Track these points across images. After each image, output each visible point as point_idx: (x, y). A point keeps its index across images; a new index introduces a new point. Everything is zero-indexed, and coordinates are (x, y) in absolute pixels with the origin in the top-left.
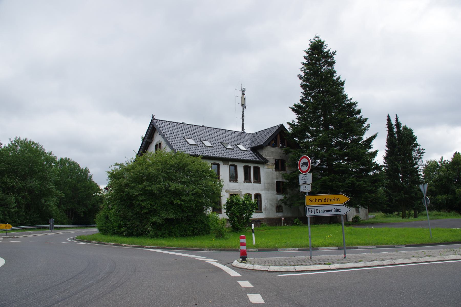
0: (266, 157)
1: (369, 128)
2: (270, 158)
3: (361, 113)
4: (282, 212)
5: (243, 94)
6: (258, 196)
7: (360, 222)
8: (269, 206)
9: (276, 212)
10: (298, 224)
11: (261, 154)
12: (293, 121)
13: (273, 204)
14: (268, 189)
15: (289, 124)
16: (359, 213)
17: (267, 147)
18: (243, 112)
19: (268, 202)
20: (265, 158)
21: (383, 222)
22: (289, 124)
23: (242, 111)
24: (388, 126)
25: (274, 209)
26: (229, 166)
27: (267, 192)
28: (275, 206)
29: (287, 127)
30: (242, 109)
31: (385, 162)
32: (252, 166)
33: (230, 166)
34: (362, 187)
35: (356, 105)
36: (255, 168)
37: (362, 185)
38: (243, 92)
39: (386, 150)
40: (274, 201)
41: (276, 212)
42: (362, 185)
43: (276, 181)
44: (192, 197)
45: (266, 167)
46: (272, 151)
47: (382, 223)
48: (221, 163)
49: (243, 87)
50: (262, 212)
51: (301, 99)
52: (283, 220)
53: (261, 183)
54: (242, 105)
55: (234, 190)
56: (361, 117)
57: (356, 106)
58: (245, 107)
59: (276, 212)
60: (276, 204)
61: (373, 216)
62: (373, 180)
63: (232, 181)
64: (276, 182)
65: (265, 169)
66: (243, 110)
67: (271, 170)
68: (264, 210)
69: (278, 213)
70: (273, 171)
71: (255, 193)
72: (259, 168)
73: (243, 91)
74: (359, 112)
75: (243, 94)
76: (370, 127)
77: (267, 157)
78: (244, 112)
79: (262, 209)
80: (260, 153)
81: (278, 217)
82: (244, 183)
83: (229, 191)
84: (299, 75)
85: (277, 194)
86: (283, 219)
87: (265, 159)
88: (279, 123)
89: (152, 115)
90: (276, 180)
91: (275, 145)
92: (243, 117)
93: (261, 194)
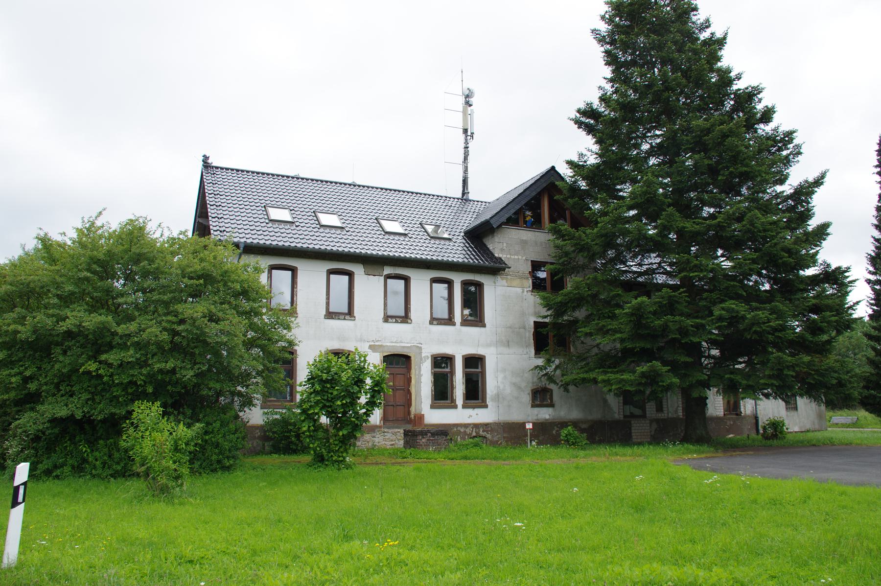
0: (505, 256)
1: (800, 158)
2: (516, 257)
3: (774, 120)
4: (552, 405)
5: (468, 104)
6: (474, 362)
7: (785, 438)
8: (508, 390)
9: (532, 406)
10: (573, 444)
11: (491, 248)
12: (581, 155)
13: (523, 385)
14: (508, 344)
15: (570, 163)
16: (797, 410)
17: (509, 230)
18: (466, 148)
19: (505, 377)
20: (500, 258)
21: (851, 444)
22: (570, 163)
23: (463, 145)
24: (879, 169)
25: (527, 398)
26: (382, 278)
27: (505, 350)
28: (529, 390)
29: (565, 171)
30: (463, 141)
31: (871, 269)
32: (457, 279)
33: (389, 277)
34: (764, 328)
35: (759, 96)
36: (465, 284)
37: (764, 323)
38: (466, 98)
39: (874, 238)
40: (526, 375)
41: (530, 405)
42: (764, 323)
43: (535, 322)
44: (130, 355)
45: (500, 281)
46: (524, 238)
47: (847, 444)
48: (358, 270)
49: (466, 86)
50: (486, 406)
51: (600, 95)
52: (530, 429)
53: (484, 326)
54: (463, 131)
55: (398, 345)
56: (776, 130)
57: (761, 99)
58: (472, 136)
59: (532, 406)
60: (531, 385)
61: (852, 419)
62: (808, 306)
63: (390, 320)
64: (532, 324)
65: (501, 288)
66: (466, 142)
67: (519, 290)
68: (492, 400)
69: (536, 410)
70: (525, 293)
71: (464, 354)
72: (479, 286)
73: (467, 96)
74: (767, 115)
75: (468, 104)
76: (800, 153)
77: (508, 256)
78: (468, 147)
79: (488, 396)
80: (488, 246)
81: (538, 420)
82: (430, 324)
83: (381, 346)
84: (593, 31)
85: (536, 356)
86: (529, 426)
87: (500, 260)
88: (544, 168)
89: (204, 156)
90: (532, 320)
91: (536, 224)
92: (466, 158)
93: (463, 356)
